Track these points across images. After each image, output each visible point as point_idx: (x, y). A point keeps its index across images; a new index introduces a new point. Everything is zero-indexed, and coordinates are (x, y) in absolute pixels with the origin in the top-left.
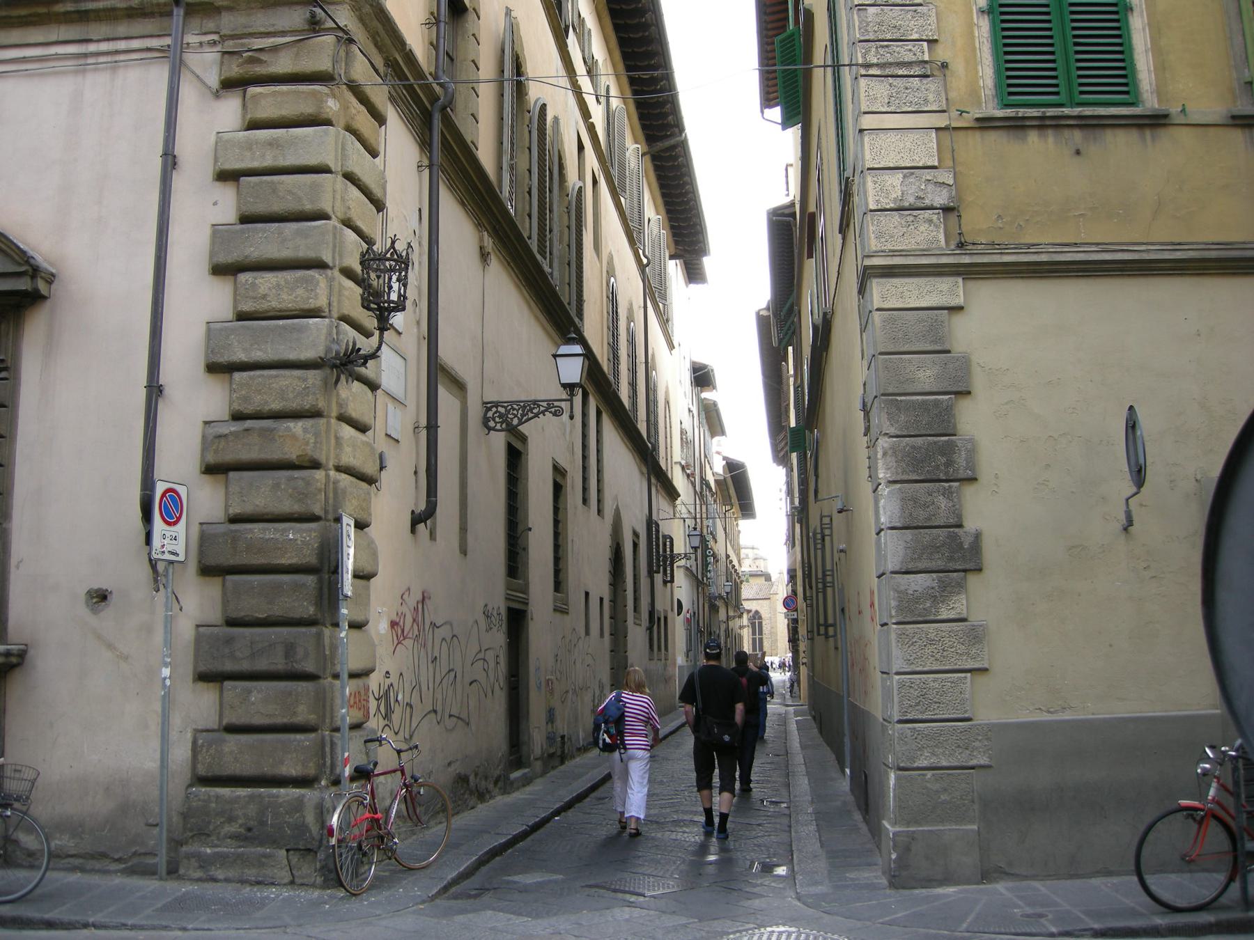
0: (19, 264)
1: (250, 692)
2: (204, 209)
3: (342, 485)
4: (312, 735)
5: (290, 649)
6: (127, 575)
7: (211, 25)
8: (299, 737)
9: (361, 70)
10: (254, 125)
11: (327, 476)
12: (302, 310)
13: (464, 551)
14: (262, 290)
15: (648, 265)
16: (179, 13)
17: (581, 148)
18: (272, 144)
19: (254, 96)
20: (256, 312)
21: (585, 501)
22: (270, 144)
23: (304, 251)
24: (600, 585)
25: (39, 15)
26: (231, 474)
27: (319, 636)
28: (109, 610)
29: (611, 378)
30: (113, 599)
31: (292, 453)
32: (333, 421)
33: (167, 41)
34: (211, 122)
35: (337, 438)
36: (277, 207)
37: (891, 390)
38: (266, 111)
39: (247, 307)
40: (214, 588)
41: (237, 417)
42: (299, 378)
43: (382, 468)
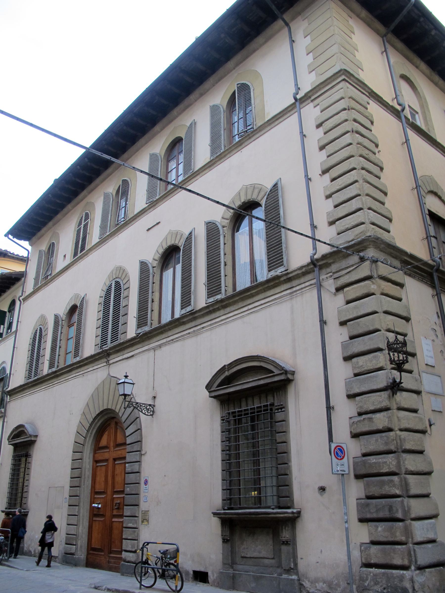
0: (281, 370)
1: (378, 527)
2: (337, 337)
3: (402, 437)
4: (404, 546)
5: (391, 508)
6: (330, 481)
7: (329, 270)
8: (399, 547)
9: (384, 269)
10: (348, 302)
11: (396, 434)
14: (361, 364)
16: (316, 269)
18: (356, 307)
20: (360, 372)
22: (354, 308)
25: (277, 283)
26: (360, 437)
27: (402, 502)
28: (326, 495)
30: (327, 489)
32: (395, 411)
33: (314, 281)
34: (335, 305)
35: (398, 417)
36: (361, 331)
39: (357, 371)
41: (360, 414)
42: (379, 396)
43: (430, 425)
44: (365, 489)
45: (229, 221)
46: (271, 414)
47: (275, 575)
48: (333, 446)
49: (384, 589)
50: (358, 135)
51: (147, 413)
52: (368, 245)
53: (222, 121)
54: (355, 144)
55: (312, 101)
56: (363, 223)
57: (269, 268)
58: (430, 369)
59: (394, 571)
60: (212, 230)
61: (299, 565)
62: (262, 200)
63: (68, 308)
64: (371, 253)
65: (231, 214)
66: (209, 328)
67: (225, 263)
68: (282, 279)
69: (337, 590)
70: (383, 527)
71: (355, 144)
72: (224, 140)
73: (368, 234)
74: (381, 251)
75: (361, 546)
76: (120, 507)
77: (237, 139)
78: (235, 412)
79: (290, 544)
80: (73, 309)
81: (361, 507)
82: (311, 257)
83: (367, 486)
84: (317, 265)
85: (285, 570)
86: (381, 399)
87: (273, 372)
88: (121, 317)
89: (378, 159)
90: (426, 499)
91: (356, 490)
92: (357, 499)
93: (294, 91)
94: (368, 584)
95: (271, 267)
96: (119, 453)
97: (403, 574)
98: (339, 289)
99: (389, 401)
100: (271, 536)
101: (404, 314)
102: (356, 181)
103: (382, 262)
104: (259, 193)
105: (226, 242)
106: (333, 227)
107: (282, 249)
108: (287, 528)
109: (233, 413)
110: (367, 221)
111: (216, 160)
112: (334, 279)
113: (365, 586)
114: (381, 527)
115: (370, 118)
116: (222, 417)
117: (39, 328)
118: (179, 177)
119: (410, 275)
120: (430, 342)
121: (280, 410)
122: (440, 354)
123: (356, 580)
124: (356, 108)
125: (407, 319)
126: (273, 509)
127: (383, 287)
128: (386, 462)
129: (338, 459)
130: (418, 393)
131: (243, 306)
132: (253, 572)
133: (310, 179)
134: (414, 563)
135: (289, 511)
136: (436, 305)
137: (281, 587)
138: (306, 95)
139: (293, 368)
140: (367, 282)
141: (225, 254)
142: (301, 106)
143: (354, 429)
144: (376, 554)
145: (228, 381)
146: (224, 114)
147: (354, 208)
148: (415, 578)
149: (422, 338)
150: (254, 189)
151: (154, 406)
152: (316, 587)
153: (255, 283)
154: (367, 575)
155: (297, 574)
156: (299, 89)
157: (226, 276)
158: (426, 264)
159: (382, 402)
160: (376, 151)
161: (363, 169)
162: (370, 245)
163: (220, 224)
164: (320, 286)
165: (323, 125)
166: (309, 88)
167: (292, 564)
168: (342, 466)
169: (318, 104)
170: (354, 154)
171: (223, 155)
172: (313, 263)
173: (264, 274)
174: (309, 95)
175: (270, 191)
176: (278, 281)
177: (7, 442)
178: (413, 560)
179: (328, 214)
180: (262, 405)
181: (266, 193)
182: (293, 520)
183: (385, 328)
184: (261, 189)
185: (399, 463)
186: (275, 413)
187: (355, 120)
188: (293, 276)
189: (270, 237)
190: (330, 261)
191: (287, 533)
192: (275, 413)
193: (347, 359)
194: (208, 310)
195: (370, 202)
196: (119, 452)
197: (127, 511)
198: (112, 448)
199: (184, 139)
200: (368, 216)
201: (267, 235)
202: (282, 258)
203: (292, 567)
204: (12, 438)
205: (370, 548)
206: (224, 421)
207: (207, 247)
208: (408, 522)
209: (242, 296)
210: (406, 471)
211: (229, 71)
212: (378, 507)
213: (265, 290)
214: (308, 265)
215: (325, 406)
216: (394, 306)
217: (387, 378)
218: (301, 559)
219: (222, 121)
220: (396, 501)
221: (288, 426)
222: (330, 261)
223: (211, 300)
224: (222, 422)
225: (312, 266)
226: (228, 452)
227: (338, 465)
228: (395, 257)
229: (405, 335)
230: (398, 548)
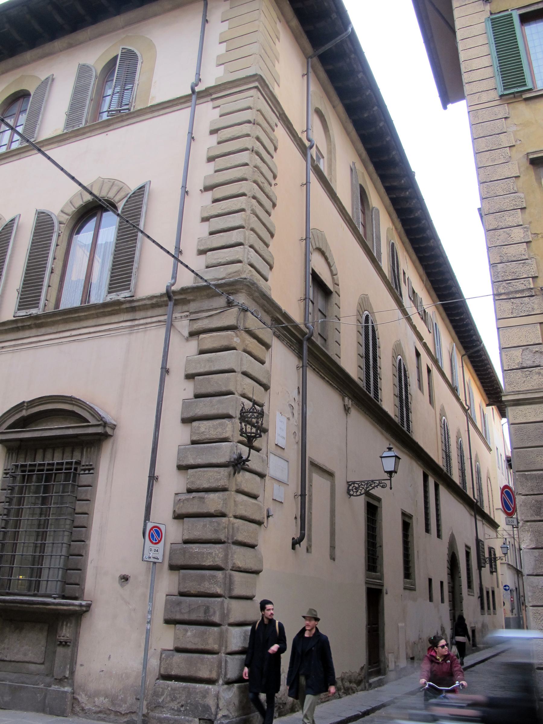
0: (99, 421)
1: (187, 631)
2: (180, 391)
3: (236, 525)
4: (215, 656)
5: (207, 610)
6: (136, 569)
7: (185, 308)
8: (209, 656)
9: (252, 323)
10: (202, 352)
11: (229, 520)
12: (219, 439)
13: (333, 558)
14: (202, 429)
15: (468, 409)
16: (171, 304)
17: (418, 354)
18: (209, 360)
19: (202, 339)
20: (199, 440)
21: (427, 530)
22: (208, 361)
23: (222, 411)
24: (441, 574)
25: (116, 310)
26: (185, 519)
27: (222, 603)
28: (128, 586)
29: (445, 469)
30: (131, 580)
31: (212, 510)
33: (165, 317)
34: (184, 352)
35: (235, 501)
37: (521, 469)
38: (208, 345)
39: (195, 438)
40: (175, 576)
42: (217, 472)
43: (268, 516)
44: (179, 584)
45: (69, 217)
46: (75, 475)
47: (42, 686)
48: (150, 525)
49: (182, 706)
50: (257, 157)
52: (240, 289)
53: (91, 88)
54: (251, 165)
55: (212, 100)
56: (240, 262)
57: (110, 288)
58: (279, 451)
59: (198, 685)
60: (44, 224)
61: (76, 673)
62: (120, 201)
64: (241, 299)
65: (74, 209)
66: (11, 349)
67: (52, 269)
68: (124, 306)
69: (121, 706)
70: (194, 631)
71: (252, 166)
72: (88, 113)
73: (243, 276)
74: (254, 300)
75: (161, 654)
77: (105, 117)
78: (25, 466)
79: (69, 646)
81: (169, 605)
82: (167, 286)
83: (182, 580)
84: (172, 299)
85: (56, 679)
86: (218, 477)
87: (88, 422)
89: (273, 193)
90: (249, 602)
91: (167, 583)
92: (167, 595)
93: (193, 80)
94: (163, 700)
95: (112, 288)
97: (209, 689)
98: (193, 334)
99: (229, 480)
100: (45, 634)
101: (264, 381)
102: (243, 210)
103: (252, 314)
104: (118, 192)
105: (59, 244)
106: (203, 257)
107: (132, 269)
108: (69, 625)
109: (22, 466)
110: (246, 261)
111: (71, 135)
112: (190, 320)
113: (159, 703)
114: (192, 630)
115: (275, 142)
116: (5, 470)
118: (13, 144)
119: (278, 337)
120: (285, 420)
121: (87, 472)
122: (292, 436)
123: (148, 695)
124: (263, 126)
125: (266, 388)
126: (55, 598)
127: (247, 342)
128: (211, 553)
129: (152, 543)
130: (262, 476)
131: (64, 329)
132: (10, 681)
133: (187, 192)
134: (223, 677)
135: (77, 602)
136: (299, 379)
137: (47, 702)
138: (207, 89)
139: (115, 421)
140: (230, 332)
141: (54, 259)
142: (198, 102)
143: (178, 509)
144: (180, 664)
145: (24, 423)
146: (95, 81)
147: (233, 241)
148: (222, 694)
149: (278, 413)
150: (112, 186)
152: (94, 703)
153: (87, 304)
154: (163, 689)
155: (72, 685)
156: (200, 80)
157: (49, 286)
158: (296, 327)
159: (220, 480)
160: (273, 182)
161: (254, 198)
162: (243, 289)
163: (57, 219)
164: (170, 326)
165: (219, 132)
166: (212, 84)
167: (68, 672)
168: (156, 552)
169: (219, 106)
170: (248, 178)
171: (81, 132)
172: (169, 295)
173: (100, 296)
174: (210, 92)
175: (133, 193)
176: (120, 308)
178: (223, 673)
179: (200, 240)
180: (65, 461)
181: (128, 194)
182: (78, 616)
183: (240, 392)
184: (121, 188)
185: (226, 555)
186: (79, 474)
187: (258, 139)
188: (139, 306)
189: (119, 250)
190: (190, 297)
191: (68, 630)
192: (79, 474)
193: (186, 421)
194: (15, 326)
195: (253, 239)
199: (32, 94)
200: (248, 254)
201: (116, 247)
202: (130, 280)
203: (67, 676)
205: (173, 656)
206: (8, 476)
207: (32, 243)
208: (224, 628)
209: (66, 317)
210: (233, 567)
211: (114, 30)
212: (193, 608)
213: (97, 316)
214: (162, 296)
215: (148, 475)
216: (254, 368)
217: (231, 452)
218: (81, 665)
219: (91, 88)
220: (215, 601)
221: (94, 493)
222: (190, 297)
223: (22, 313)
224: (5, 476)
225: (166, 299)
226: (5, 517)
227: (151, 550)
228: (267, 312)
229: (261, 406)
230: (207, 658)
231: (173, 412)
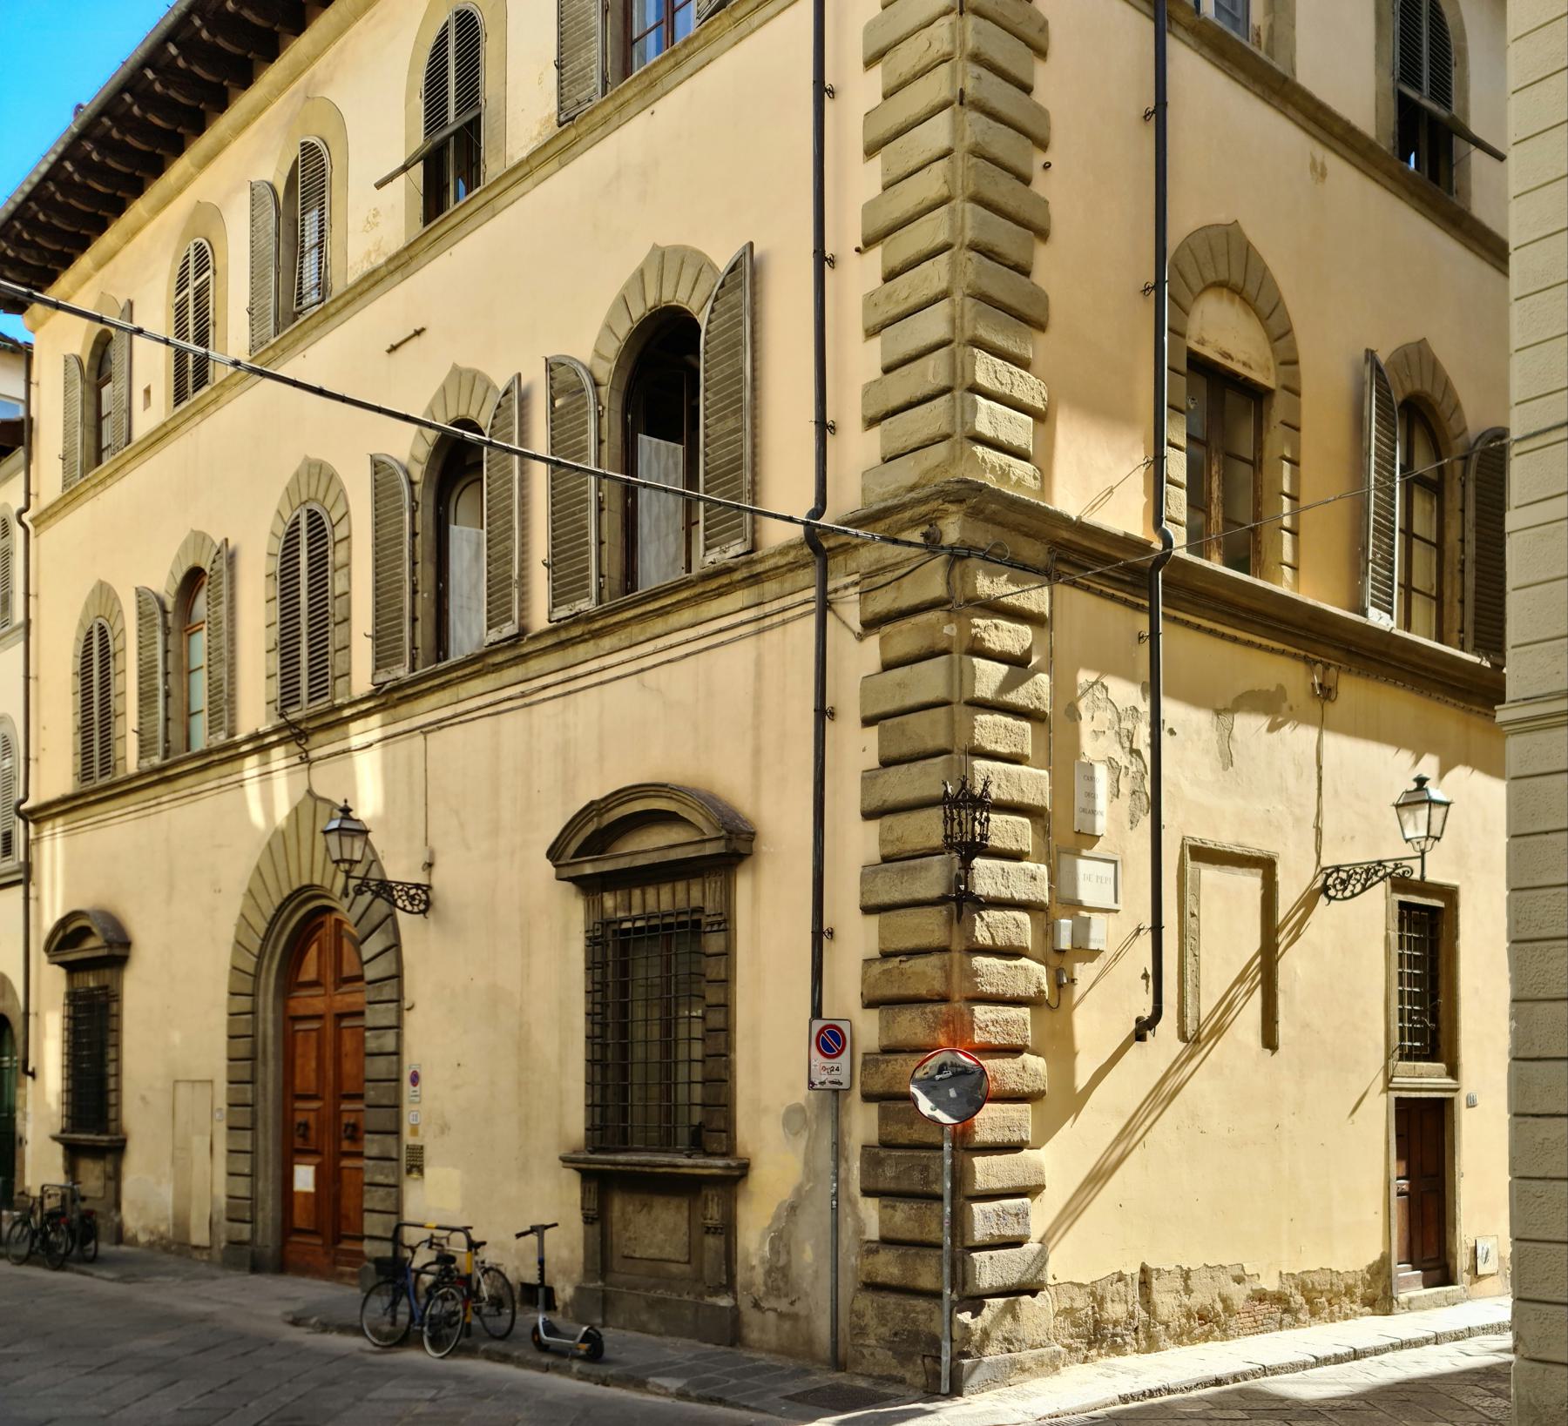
2: (856, 748)
39: (889, 850)
51: (409, 908)
63: (179, 577)
76: (355, 1133)
80: (193, 580)
88: (331, 626)
96: (347, 999)
98: (871, 624)
117: (96, 627)
144: (888, 1267)
145: (600, 842)
151: (429, 887)
177: (44, 957)
196: (349, 999)
197: (372, 1146)
198: (331, 987)
204: (59, 948)
231: (846, 798)
